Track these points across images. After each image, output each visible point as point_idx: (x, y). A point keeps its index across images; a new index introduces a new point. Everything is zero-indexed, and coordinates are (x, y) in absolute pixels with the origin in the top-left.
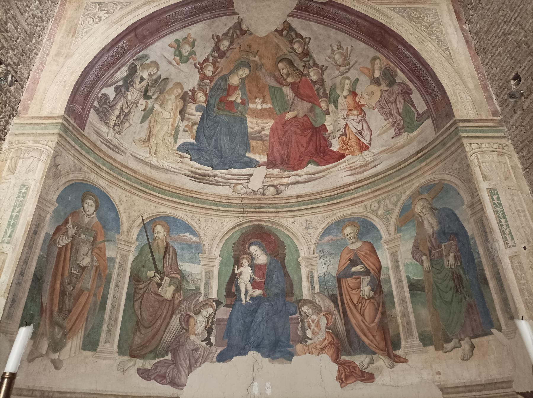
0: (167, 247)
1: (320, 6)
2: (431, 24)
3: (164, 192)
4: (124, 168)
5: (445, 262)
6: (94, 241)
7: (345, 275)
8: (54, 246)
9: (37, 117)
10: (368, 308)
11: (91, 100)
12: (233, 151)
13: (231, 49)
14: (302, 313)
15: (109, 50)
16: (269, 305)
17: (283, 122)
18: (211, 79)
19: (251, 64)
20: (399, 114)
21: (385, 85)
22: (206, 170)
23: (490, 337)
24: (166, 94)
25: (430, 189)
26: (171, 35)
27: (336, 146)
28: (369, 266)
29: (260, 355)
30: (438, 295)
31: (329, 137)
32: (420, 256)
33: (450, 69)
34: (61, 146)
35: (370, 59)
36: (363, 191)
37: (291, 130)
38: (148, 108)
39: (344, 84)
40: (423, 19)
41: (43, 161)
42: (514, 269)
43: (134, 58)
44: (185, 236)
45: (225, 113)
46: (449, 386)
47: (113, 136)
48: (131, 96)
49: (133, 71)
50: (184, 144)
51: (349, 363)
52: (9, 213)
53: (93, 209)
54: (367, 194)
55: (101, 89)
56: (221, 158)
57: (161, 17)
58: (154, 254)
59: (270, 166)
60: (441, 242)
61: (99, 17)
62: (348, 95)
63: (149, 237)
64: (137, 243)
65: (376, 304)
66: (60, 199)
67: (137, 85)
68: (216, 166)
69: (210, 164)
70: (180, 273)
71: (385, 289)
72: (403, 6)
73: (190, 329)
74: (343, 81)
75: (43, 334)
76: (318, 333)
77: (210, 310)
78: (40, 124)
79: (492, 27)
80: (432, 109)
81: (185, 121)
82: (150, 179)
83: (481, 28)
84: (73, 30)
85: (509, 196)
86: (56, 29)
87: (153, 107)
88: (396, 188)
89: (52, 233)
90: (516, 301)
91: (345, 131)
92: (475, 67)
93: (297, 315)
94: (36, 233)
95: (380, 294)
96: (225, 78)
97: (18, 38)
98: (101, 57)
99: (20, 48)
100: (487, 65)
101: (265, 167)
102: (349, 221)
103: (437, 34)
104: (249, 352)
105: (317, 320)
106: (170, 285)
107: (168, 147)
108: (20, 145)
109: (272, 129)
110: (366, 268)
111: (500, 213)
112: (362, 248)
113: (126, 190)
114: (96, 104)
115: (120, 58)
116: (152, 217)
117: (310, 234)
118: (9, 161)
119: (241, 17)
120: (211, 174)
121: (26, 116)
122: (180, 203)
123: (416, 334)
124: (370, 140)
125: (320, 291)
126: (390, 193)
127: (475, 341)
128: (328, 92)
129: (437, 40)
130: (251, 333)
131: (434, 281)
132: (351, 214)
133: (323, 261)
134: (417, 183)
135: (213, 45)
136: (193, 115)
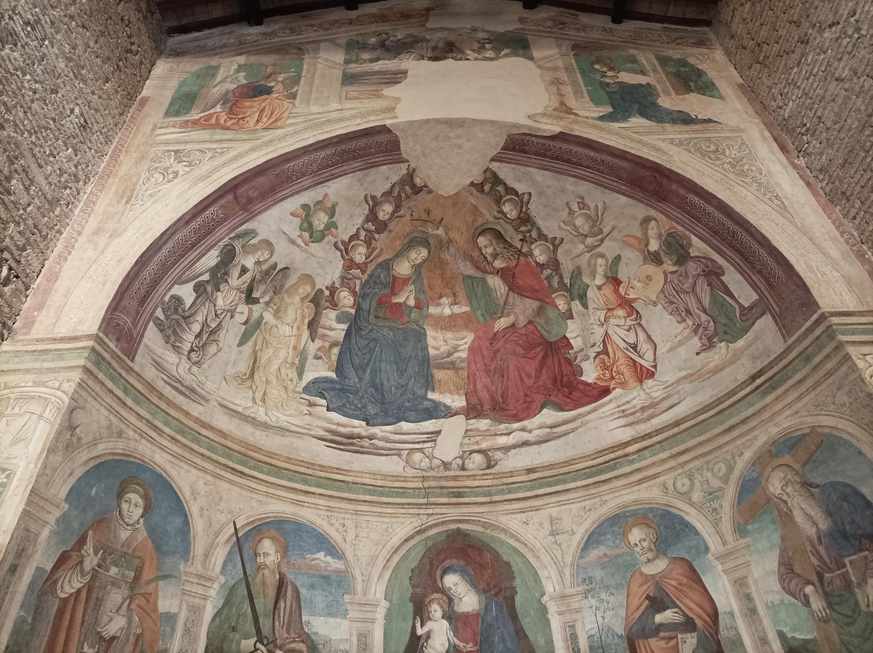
0: (281, 584)
1: (544, 141)
3: (277, 471)
4: (205, 428)
5: (860, 597)
6: (137, 578)
7: (643, 630)
8: (51, 597)
9: (48, 339)
11: (149, 307)
12: (402, 390)
13: (397, 217)
15: (188, 223)
17: (491, 335)
18: (362, 268)
19: (432, 241)
21: (670, 262)
22: (355, 427)
25: (794, 445)
26: (296, 196)
27: (590, 374)
28: (690, 609)
31: (576, 358)
32: (800, 586)
34: (86, 390)
36: (654, 455)
37: (506, 349)
39: (595, 266)
40: (723, 153)
41: (47, 420)
43: (231, 236)
44: (318, 559)
45: (388, 324)
47: (186, 370)
48: (222, 300)
49: (228, 256)
50: (315, 382)
53: (139, 512)
54: (663, 461)
55: (170, 288)
56: (383, 403)
57: (279, 170)
58: (255, 601)
61: (174, 172)
62: (604, 284)
63: (247, 566)
64: (222, 579)
66: (75, 494)
67: (235, 280)
68: (373, 418)
69: (362, 416)
72: (686, 136)
74: (593, 261)
78: (50, 351)
79: (853, 156)
80: (769, 297)
81: (317, 340)
82: (251, 448)
83: (830, 161)
84: (128, 193)
87: (261, 317)
88: (720, 447)
89: (49, 567)
91: (605, 346)
92: (834, 222)
94: (15, 570)
96: (386, 266)
97: (29, 205)
98: (173, 234)
99: (30, 222)
100: (855, 218)
101: (463, 417)
102: (634, 515)
103: (752, 174)
107: (286, 388)
108: (7, 391)
109: (471, 349)
110: (685, 615)
112: (671, 572)
113: (204, 470)
114: (159, 313)
115: (207, 235)
116: (253, 522)
117: (560, 545)
119: (413, 165)
120: (364, 434)
121: (28, 337)
124: (655, 359)
126: (710, 457)
128: (567, 281)
131: (841, 640)
132: (636, 502)
133: (593, 602)
134: (763, 437)
135: (366, 212)
136: (331, 329)
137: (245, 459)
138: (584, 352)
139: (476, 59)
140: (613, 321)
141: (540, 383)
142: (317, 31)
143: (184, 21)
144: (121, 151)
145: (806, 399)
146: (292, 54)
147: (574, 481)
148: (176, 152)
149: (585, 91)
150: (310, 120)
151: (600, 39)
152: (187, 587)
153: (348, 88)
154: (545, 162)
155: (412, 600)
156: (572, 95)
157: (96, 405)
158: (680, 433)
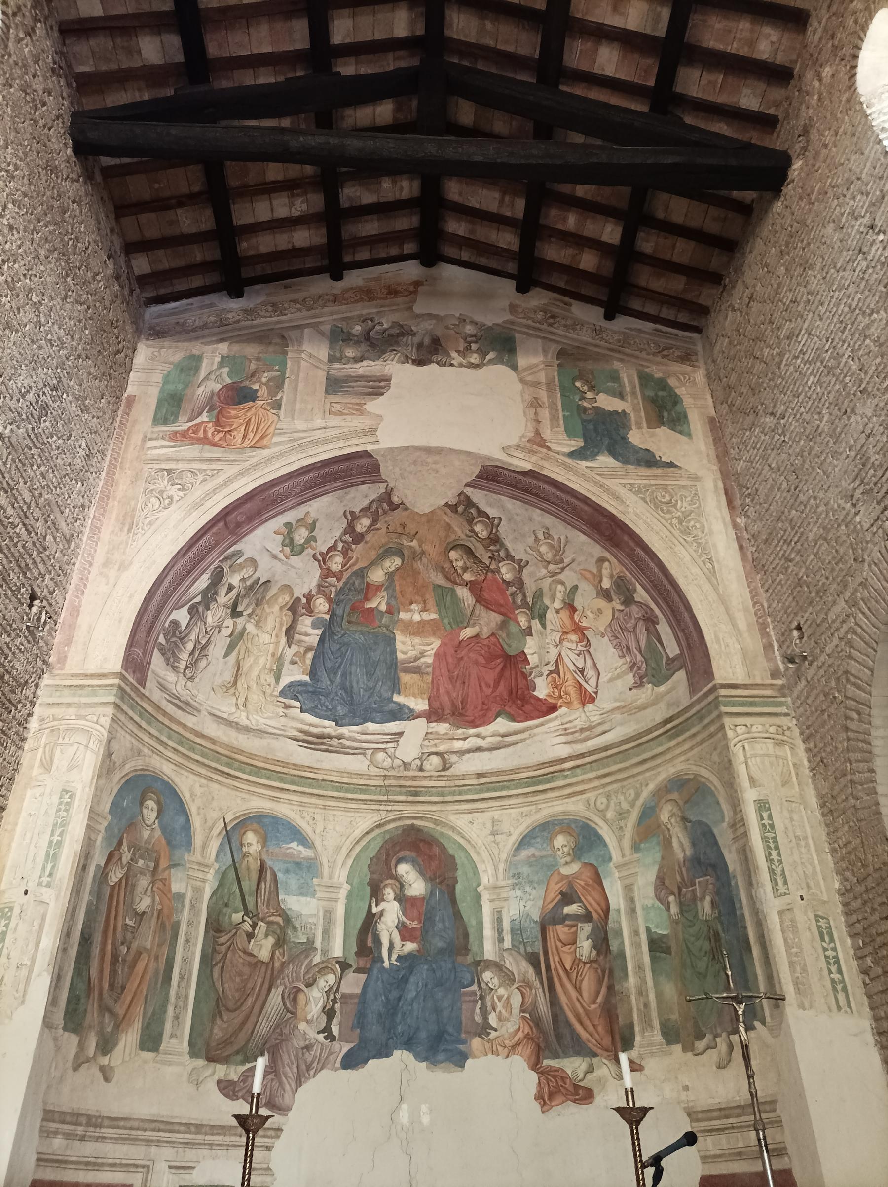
0: (262, 868)
1: (516, 475)
2: (687, 515)
3: (257, 771)
4: (198, 737)
6: (156, 867)
7: (554, 918)
10: (586, 978)
14: (483, 985)
15: (185, 554)
16: (428, 970)
18: (338, 576)
19: (406, 552)
20: (641, 652)
24: (266, 606)
26: (280, 517)
27: (542, 690)
28: (591, 905)
29: (411, 1057)
30: (688, 960)
31: (531, 673)
33: (712, 596)
35: (595, 560)
36: (584, 773)
37: (469, 657)
38: (237, 631)
40: (675, 506)
42: (783, 931)
45: (359, 628)
46: (699, 1109)
48: (211, 618)
49: (218, 577)
50: (291, 685)
51: (556, 1071)
52: (47, 837)
53: (154, 815)
54: (590, 780)
56: (351, 704)
59: (433, 718)
60: (694, 876)
61: (169, 497)
62: (562, 608)
63: (235, 854)
64: (217, 866)
65: (599, 971)
67: (223, 598)
68: (342, 719)
71: (614, 946)
72: (646, 482)
73: (299, 1012)
74: (553, 586)
75: (90, 1027)
76: (508, 1020)
77: (331, 979)
81: (293, 646)
82: (235, 751)
84: (129, 520)
85: (786, 813)
86: (101, 518)
87: (244, 629)
88: (634, 776)
90: (783, 981)
91: (557, 665)
92: (751, 592)
93: (475, 987)
95: (606, 954)
96: (361, 574)
98: (173, 566)
101: (425, 720)
103: (695, 532)
104: (395, 1051)
105: (506, 996)
106: (267, 936)
107: (265, 693)
108: (56, 723)
109: (437, 655)
110: (586, 909)
111: (771, 841)
113: (199, 775)
114: (162, 640)
117: (498, 844)
118: (41, 750)
119: (391, 485)
120: (333, 733)
121: (63, 672)
122: (282, 789)
123: (656, 1023)
125: (513, 945)
126: (625, 783)
128: (529, 600)
129: (695, 544)
132: (564, 813)
133: (519, 893)
134: (666, 772)
135: (345, 525)
136: (307, 635)
138: (539, 669)
139: (461, 365)
140: (566, 644)
141: (497, 693)
142: (299, 310)
143: (162, 291)
144: (116, 467)
145: (695, 751)
146: (276, 344)
147: (516, 788)
148: (169, 471)
149: (561, 418)
150: (295, 440)
151: (587, 344)
152: (190, 873)
153: (332, 398)
154: (517, 493)
155: (369, 884)
156: (548, 422)
157: (123, 733)
158: (607, 757)
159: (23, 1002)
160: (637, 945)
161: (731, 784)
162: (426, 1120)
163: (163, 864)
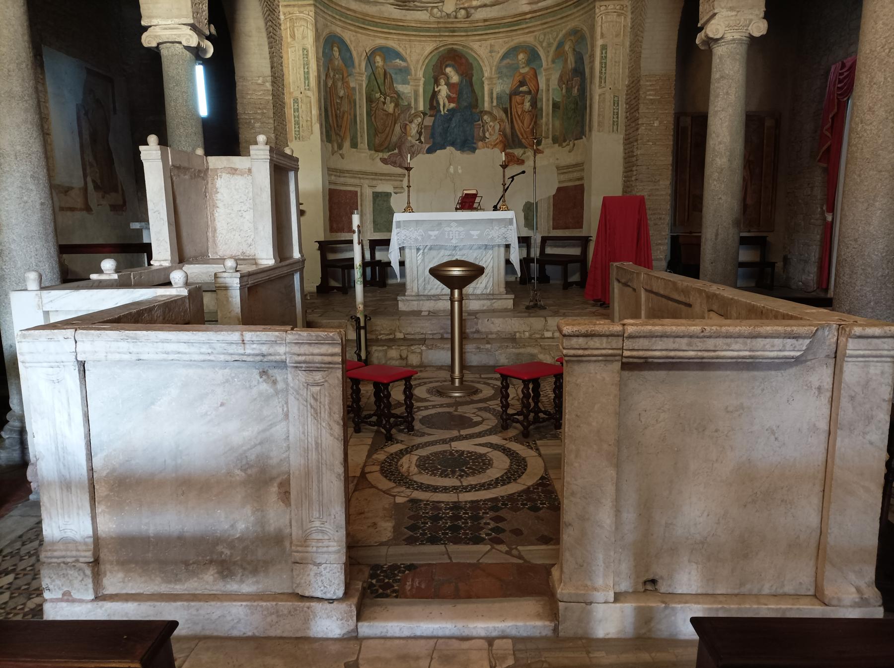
0: (385, 73)
3: (376, 24)
6: (343, 77)
23: (581, 140)
54: (538, 25)
70: (397, 93)
71: (539, 106)
77: (420, 120)
93: (480, 122)
106: (391, 103)
108: (291, 15)
110: (529, 89)
118: (288, 29)
123: (551, 137)
125: (497, 104)
126: (553, 29)
127: (576, 142)
130: (448, 134)
132: (525, 42)
133: (501, 81)
134: (571, 25)
137: (364, 21)
159: (312, 133)
160: (548, 105)
161: (593, 37)
162: (460, 171)
163: (345, 75)
